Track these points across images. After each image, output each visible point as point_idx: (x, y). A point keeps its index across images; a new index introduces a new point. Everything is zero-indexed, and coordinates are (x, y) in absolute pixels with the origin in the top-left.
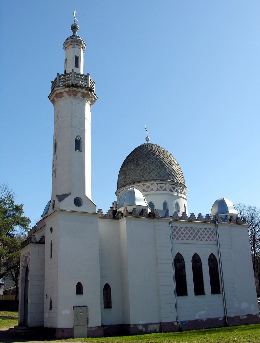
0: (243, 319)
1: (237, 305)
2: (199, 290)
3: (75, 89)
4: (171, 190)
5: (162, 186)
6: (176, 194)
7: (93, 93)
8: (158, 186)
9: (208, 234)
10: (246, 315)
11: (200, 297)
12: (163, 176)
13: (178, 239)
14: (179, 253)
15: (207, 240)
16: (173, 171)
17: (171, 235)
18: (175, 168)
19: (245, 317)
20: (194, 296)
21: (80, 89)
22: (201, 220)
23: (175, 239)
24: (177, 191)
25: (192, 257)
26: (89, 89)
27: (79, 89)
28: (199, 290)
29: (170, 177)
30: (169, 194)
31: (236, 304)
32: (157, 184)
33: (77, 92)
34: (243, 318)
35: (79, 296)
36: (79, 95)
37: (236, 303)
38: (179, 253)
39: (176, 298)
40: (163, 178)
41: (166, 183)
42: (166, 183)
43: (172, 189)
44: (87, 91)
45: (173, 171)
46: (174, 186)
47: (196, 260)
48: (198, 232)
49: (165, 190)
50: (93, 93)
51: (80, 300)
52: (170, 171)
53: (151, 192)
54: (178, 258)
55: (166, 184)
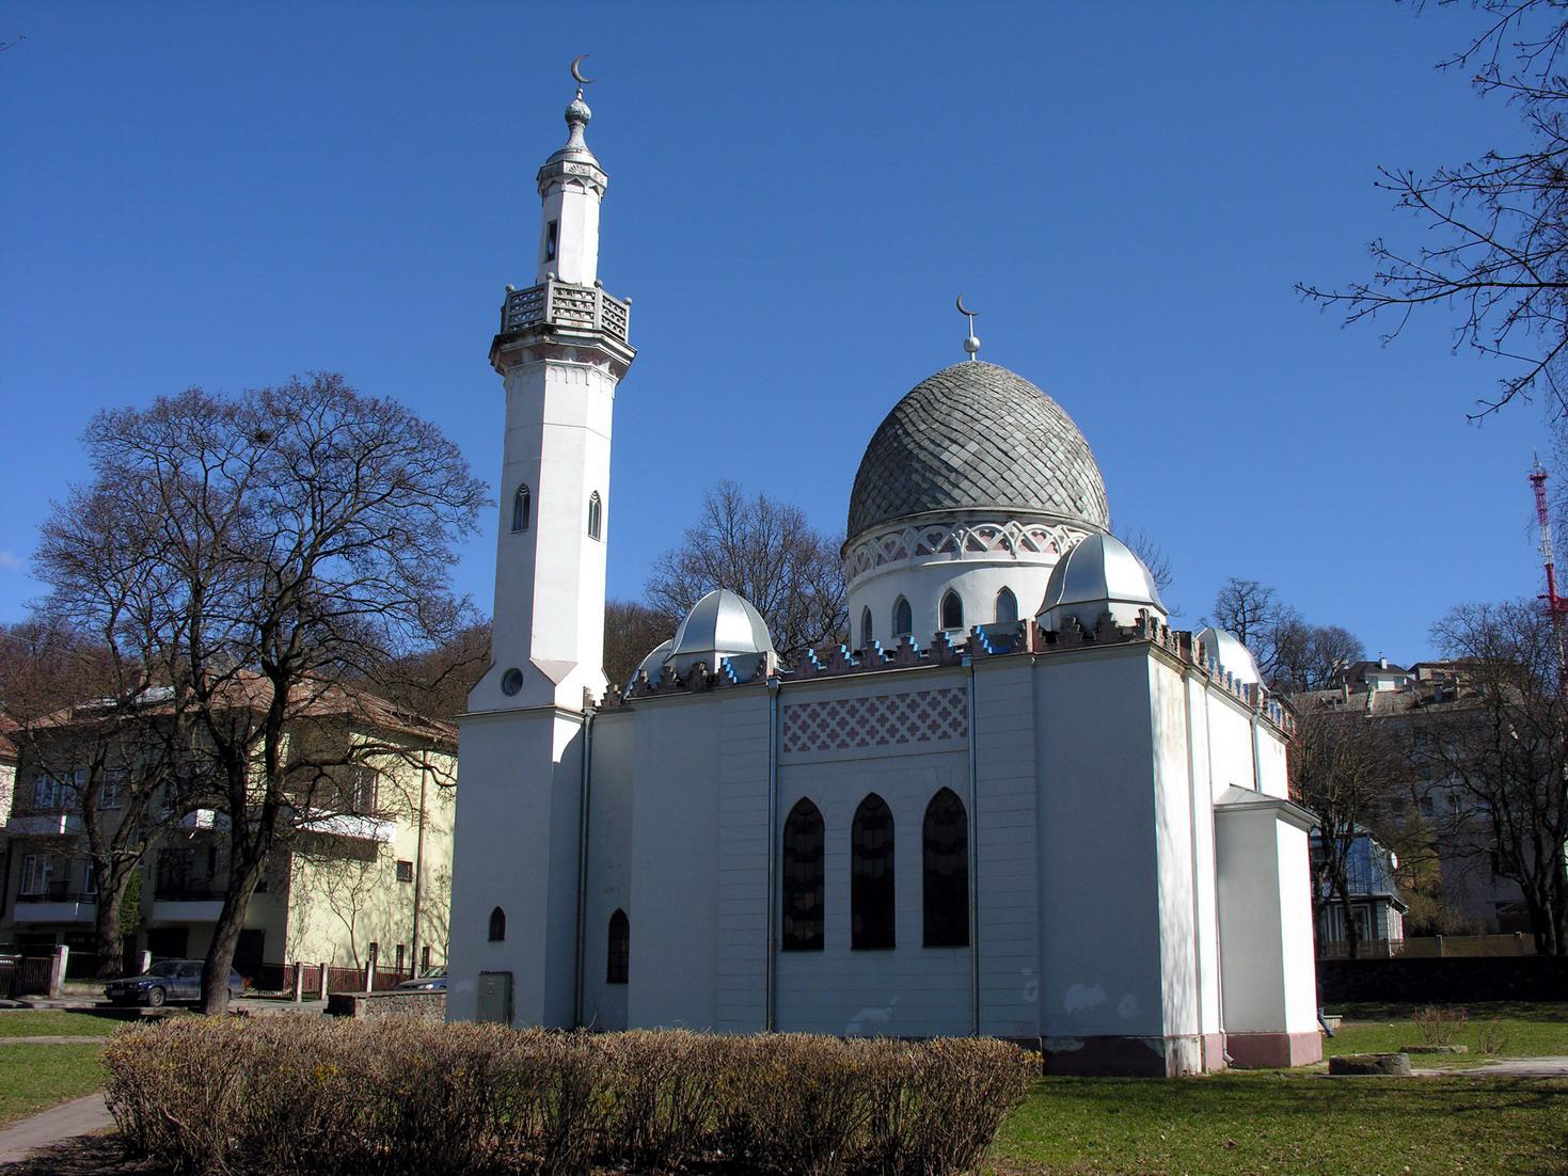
0: (1064, 1051)
1: (1031, 994)
2: (874, 930)
3: (507, 346)
4: (922, 551)
5: (889, 541)
6: (946, 560)
7: (561, 332)
8: (879, 547)
9: (822, 734)
10: (1078, 1039)
11: (872, 960)
12: (898, 502)
13: (804, 748)
14: (805, 800)
15: (929, 739)
16: (944, 471)
17: (970, 705)
18: (955, 457)
19: (1077, 1046)
20: (849, 951)
21: (520, 342)
22: (907, 663)
23: (814, 748)
24: (951, 547)
25: (858, 809)
26: (540, 329)
27: (517, 343)
28: (874, 930)
29: (924, 498)
30: (913, 569)
31: (1026, 992)
32: (918, 529)
33: (517, 353)
34: (1064, 1048)
35: (498, 944)
36: (526, 356)
37: (1028, 985)
38: (805, 800)
39: (775, 960)
40: (898, 510)
41: (902, 527)
42: (902, 527)
43: (927, 544)
44: (539, 338)
45: (944, 471)
46: (934, 530)
47: (873, 818)
48: (909, 711)
49: (901, 554)
50: (561, 332)
51: (498, 957)
52: (927, 474)
53: (900, 563)
54: (803, 817)
55: (900, 532)
